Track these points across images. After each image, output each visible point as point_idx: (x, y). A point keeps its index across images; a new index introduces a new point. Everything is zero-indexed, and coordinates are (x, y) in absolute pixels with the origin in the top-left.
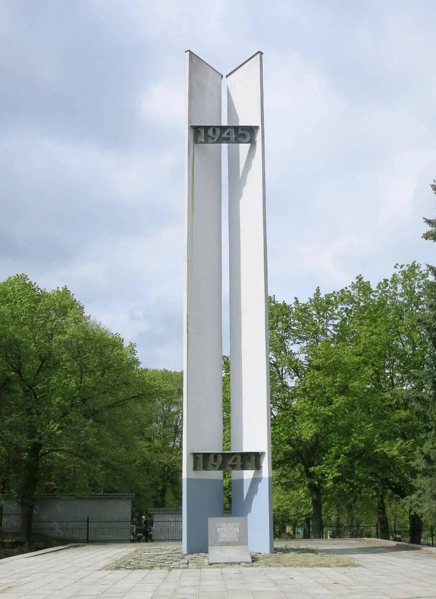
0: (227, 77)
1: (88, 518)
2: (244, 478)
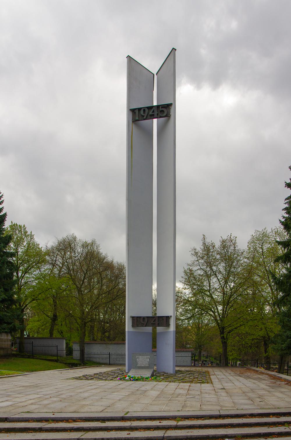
0: (157, 74)
1: (109, 353)
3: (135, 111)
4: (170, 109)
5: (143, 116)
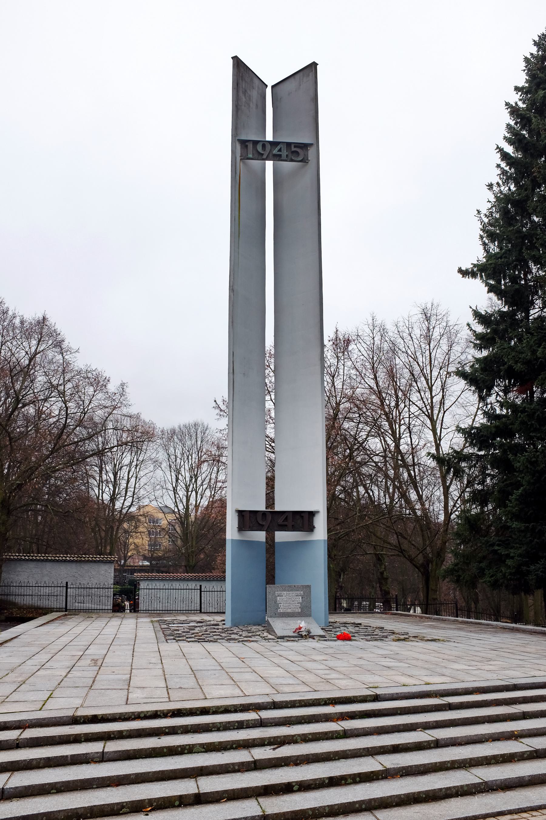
0: (273, 87)
1: (67, 583)
2: (231, 538)
3: (247, 144)
4: (307, 150)
5: (262, 154)
